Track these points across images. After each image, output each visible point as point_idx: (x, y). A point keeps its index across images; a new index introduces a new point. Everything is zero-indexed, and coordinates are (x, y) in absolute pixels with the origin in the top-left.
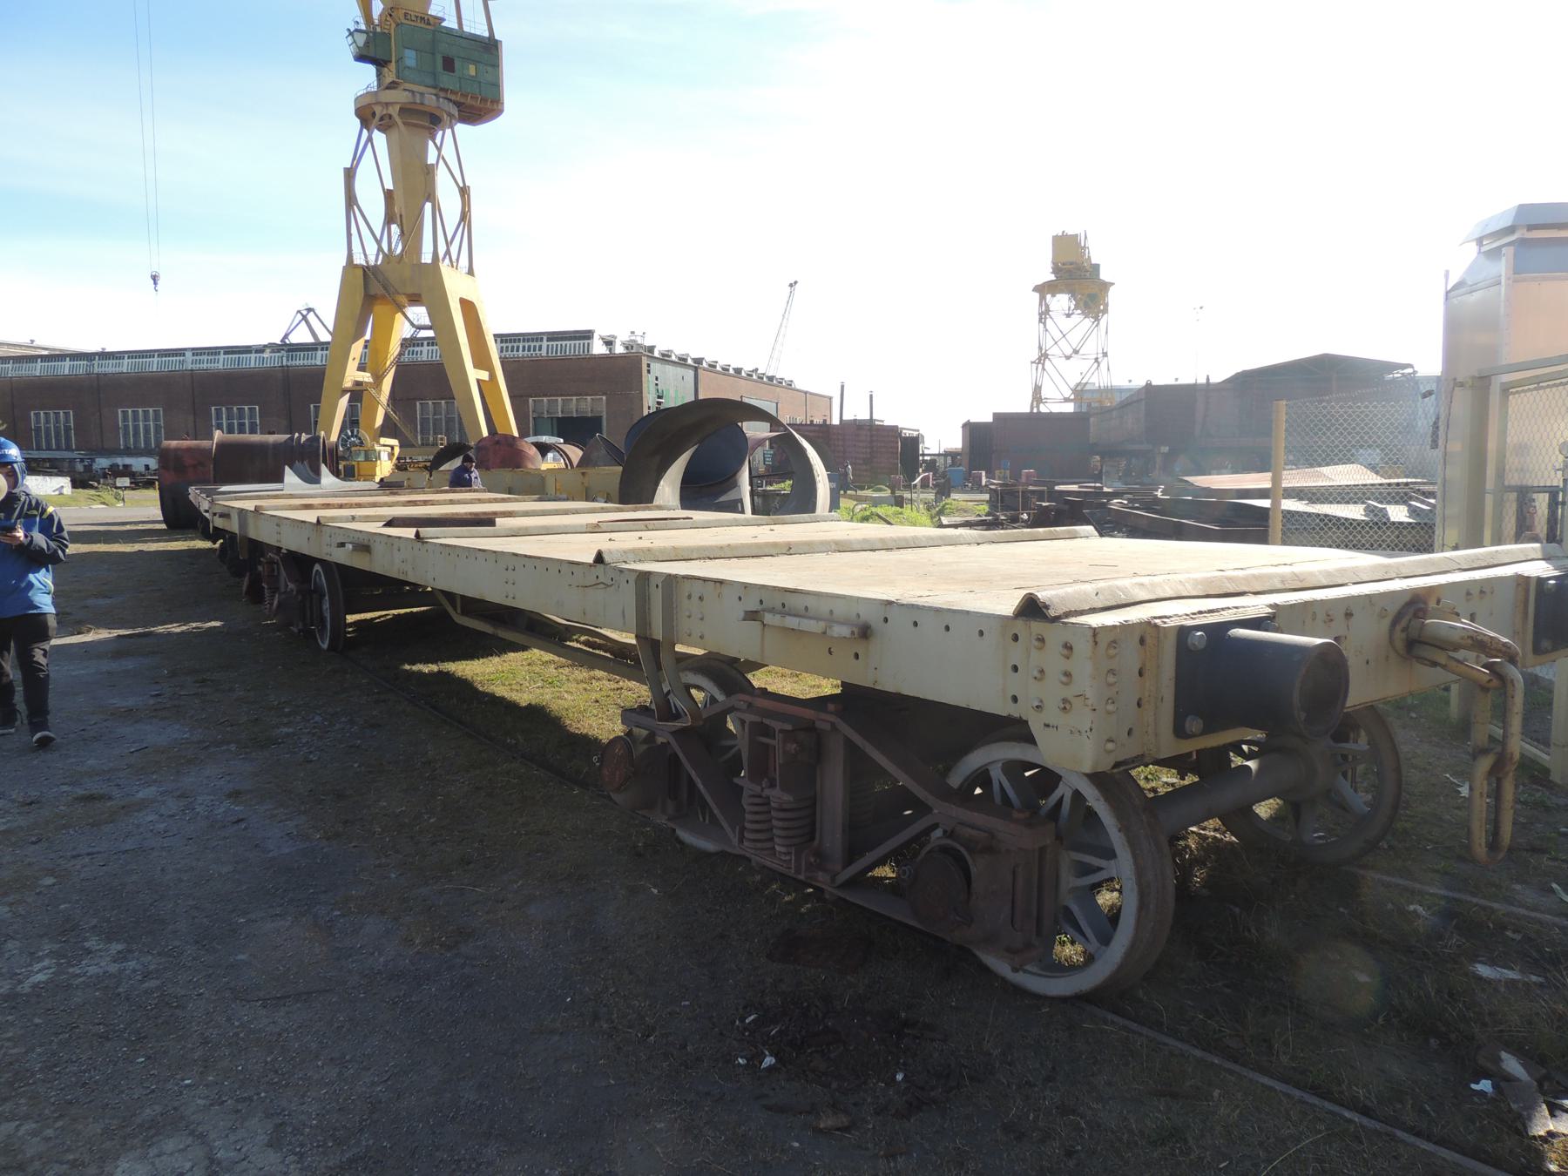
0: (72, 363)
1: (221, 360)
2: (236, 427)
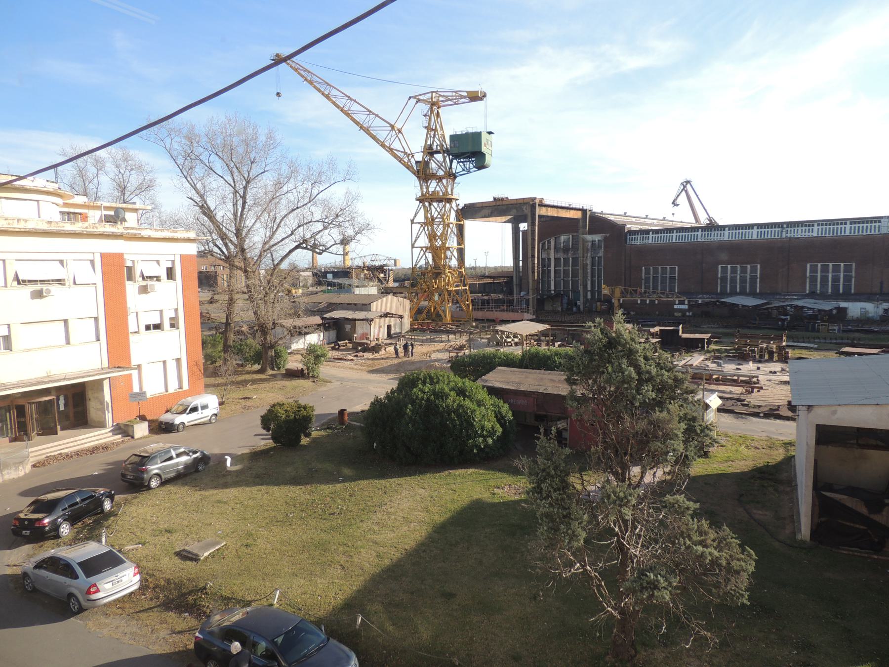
0: (678, 234)
1: (650, 238)
2: (729, 280)
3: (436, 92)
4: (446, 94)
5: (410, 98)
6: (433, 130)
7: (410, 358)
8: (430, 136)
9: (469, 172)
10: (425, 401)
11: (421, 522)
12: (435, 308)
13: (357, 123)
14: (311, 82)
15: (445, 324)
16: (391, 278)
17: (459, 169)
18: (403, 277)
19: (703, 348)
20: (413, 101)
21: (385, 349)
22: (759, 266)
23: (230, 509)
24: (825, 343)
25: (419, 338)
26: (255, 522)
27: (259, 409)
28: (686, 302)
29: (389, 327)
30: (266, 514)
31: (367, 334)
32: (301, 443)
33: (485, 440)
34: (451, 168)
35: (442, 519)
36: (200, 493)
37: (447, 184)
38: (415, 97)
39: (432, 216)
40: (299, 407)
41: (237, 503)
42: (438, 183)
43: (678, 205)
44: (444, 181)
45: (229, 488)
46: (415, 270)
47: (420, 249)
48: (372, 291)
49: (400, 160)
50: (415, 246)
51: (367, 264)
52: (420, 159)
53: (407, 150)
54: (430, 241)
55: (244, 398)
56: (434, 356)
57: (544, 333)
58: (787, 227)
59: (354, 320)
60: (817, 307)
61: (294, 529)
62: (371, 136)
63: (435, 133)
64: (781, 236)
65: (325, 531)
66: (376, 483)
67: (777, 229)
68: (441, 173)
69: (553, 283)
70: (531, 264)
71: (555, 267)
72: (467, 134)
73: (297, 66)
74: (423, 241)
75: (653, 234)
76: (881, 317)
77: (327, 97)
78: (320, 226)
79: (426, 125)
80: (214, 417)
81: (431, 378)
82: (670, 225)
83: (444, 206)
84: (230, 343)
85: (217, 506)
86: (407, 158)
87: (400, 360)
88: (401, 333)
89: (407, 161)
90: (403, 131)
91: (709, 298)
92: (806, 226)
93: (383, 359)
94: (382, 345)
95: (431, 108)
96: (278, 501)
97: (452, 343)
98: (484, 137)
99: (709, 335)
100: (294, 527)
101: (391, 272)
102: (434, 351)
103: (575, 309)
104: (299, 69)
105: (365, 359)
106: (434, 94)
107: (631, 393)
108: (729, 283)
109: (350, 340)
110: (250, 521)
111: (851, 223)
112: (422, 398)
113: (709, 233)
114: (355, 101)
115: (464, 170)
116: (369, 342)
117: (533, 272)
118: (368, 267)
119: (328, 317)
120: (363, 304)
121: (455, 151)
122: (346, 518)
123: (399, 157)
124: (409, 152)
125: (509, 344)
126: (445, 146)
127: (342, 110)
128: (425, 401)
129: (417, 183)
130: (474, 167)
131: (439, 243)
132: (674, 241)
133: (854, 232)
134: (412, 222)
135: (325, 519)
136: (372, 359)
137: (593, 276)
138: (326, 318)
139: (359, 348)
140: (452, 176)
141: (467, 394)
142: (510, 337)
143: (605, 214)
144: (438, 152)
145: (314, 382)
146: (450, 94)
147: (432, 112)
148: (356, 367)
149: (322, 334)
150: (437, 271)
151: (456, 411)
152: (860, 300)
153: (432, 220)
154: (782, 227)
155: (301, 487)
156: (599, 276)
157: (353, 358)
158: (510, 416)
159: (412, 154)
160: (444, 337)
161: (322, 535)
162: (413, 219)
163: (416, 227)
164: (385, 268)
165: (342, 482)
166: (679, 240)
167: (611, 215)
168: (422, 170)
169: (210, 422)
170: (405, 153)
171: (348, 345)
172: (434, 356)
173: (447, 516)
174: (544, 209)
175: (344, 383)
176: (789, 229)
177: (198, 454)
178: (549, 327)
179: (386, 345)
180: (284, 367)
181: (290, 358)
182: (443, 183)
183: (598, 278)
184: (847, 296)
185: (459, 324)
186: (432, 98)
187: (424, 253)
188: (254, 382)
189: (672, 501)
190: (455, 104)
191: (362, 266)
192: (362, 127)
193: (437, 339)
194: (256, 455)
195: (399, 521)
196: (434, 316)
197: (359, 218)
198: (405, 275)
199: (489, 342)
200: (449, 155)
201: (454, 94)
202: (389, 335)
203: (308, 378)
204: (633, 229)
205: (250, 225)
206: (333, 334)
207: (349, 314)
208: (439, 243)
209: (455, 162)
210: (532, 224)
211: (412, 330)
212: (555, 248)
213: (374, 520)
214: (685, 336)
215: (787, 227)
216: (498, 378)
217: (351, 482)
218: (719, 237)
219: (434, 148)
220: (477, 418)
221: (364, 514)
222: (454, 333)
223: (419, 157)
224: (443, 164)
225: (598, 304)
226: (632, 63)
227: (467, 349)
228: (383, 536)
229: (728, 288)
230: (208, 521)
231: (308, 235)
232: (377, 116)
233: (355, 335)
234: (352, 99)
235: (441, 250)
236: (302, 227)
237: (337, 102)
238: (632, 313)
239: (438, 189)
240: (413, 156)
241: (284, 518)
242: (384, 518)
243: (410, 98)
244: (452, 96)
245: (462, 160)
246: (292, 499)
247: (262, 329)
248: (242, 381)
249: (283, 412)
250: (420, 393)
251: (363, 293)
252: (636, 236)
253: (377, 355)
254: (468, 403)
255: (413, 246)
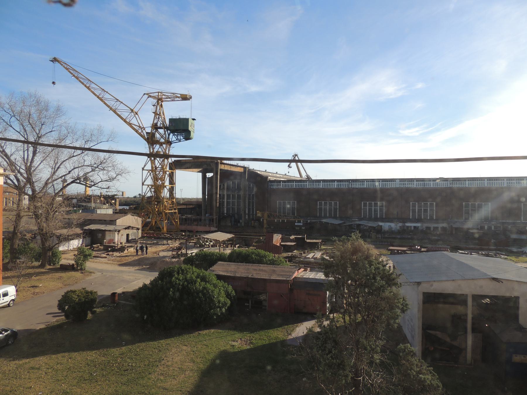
2: (323, 210)
3: (161, 93)
4: (167, 94)
5: (144, 94)
6: (158, 114)
7: (145, 256)
8: (156, 118)
9: (180, 141)
10: (181, 286)
11: (192, 370)
12: (156, 222)
13: (108, 106)
14: (77, 78)
15: (163, 234)
16: (118, 203)
17: (174, 139)
18: (124, 203)
19: (318, 247)
20: (146, 96)
21: (128, 250)
22: (338, 203)
23: (44, 373)
24: (382, 244)
25: (148, 242)
26: (67, 382)
27: (45, 294)
28: (302, 222)
29: (128, 235)
30: (74, 375)
31: (113, 240)
32: (87, 319)
33: (221, 310)
34: (169, 138)
35: (206, 367)
36: (14, 362)
37: (166, 147)
38: (147, 94)
39: (156, 166)
40: (87, 292)
41: (48, 368)
42: (160, 146)
43: (291, 167)
44: (164, 146)
45: (38, 356)
46: (144, 199)
47: (147, 186)
48: (109, 211)
49: (137, 131)
50: (145, 184)
51: (103, 194)
52: (150, 131)
53: (141, 125)
54: (154, 182)
55: (33, 287)
56: (162, 254)
57: (229, 240)
58: (352, 182)
59: (105, 231)
60: (369, 225)
61: (100, 385)
62: (118, 116)
63: (159, 117)
64: (349, 186)
65: (125, 384)
66: (151, 344)
67: (347, 183)
68: (162, 140)
69: (225, 209)
70: (215, 197)
71: (227, 199)
72: (180, 119)
73: (68, 67)
74: (149, 181)
75: (283, 183)
76: (399, 230)
77: (88, 88)
78: (89, 169)
79: (154, 111)
80: (11, 302)
81: (183, 271)
82: (289, 178)
83: (163, 161)
84: (16, 246)
85: (33, 372)
86: (141, 130)
87: (139, 257)
88: (135, 239)
89: (140, 132)
90: (139, 113)
91: (314, 220)
92: (361, 182)
93: (127, 256)
94: (125, 247)
95: (158, 102)
96: (81, 364)
97: (171, 246)
98: (190, 121)
99: (321, 240)
100: (99, 383)
101: (117, 200)
102: (160, 251)
103: (239, 224)
104: (70, 69)
105: (115, 257)
106: (160, 94)
107: (371, 281)
108: (323, 211)
109: (102, 244)
110: (63, 382)
111: (382, 182)
112: (179, 284)
113: (313, 183)
114: (107, 92)
115: (177, 140)
116: (116, 245)
117: (217, 203)
118: (104, 196)
119: (87, 229)
120: (110, 220)
121: (172, 128)
122: (138, 372)
123: (136, 129)
124: (142, 127)
125: (207, 246)
126: (165, 125)
127: (98, 97)
128: (181, 286)
129: (147, 145)
130: (184, 138)
131: (160, 183)
132: (294, 187)
133: (384, 186)
134: (143, 169)
135: (122, 375)
136: (119, 257)
137: (249, 205)
138: (85, 230)
139: (110, 249)
140: (169, 143)
141: (207, 280)
142: (208, 242)
143: (255, 170)
144: (160, 128)
145: (82, 273)
146: (170, 94)
147: (158, 104)
148: (109, 262)
149: (81, 240)
150: (157, 199)
151: (202, 291)
152: (388, 222)
153: (155, 169)
154: (349, 182)
155: (96, 351)
156: (253, 206)
157: (106, 256)
158: (234, 293)
159: (144, 128)
160: (165, 242)
161: (124, 387)
162: (144, 168)
163: (145, 172)
164: (115, 197)
165: (125, 345)
166: (297, 187)
167: (259, 171)
168: (150, 138)
169: (9, 305)
170: (140, 127)
171: (100, 247)
172: (161, 254)
173: (208, 364)
174: (223, 165)
175: (104, 273)
176: (353, 183)
177: (9, 332)
178: (234, 236)
179: (128, 247)
180: (58, 263)
181: (63, 256)
182: (163, 147)
183: (252, 207)
184: (382, 220)
185: (172, 235)
186: (158, 96)
187: (150, 189)
188: (38, 274)
189: (403, 347)
190: (173, 101)
191: (100, 195)
192: (111, 109)
193: (159, 243)
194: (51, 329)
195: (177, 371)
196: (154, 228)
197: (119, 166)
198: (126, 202)
199: (195, 245)
200: (167, 130)
201: (172, 95)
202: (128, 241)
203: (77, 270)
204: (271, 179)
205: (36, 166)
206: (88, 240)
207: (102, 227)
208: (160, 183)
209: (171, 134)
210: (216, 174)
211: (143, 237)
212: (227, 189)
213: (159, 372)
214: (308, 241)
215: (352, 182)
216: (220, 269)
217: (132, 345)
218: (318, 186)
219: (159, 125)
220: (216, 295)
221: (150, 368)
222: (171, 239)
223: (149, 130)
224: (164, 136)
225: (253, 222)
226: (254, 89)
227: (183, 249)
228: (169, 383)
229: (323, 214)
230: (28, 385)
231: (81, 174)
232: (122, 103)
233: (105, 241)
234: (105, 91)
235: (161, 187)
236: (77, 169)
237: (95, 92)
238: (272, 227)
239: (160, 150)
240: (144, 129)
241: (89, 376)
242: (165, 369)
243: (144, 94)
244: (171, 96)
245: (176, 134)
246: (92, 361)
247: (44, 236)
248: (28, 274)
249: (76, 297)
250: (177, 280)
251: (103, 213)
252: (274, 184)
253: (122, 254)
254: (208, 285)
255: (143, 184)
